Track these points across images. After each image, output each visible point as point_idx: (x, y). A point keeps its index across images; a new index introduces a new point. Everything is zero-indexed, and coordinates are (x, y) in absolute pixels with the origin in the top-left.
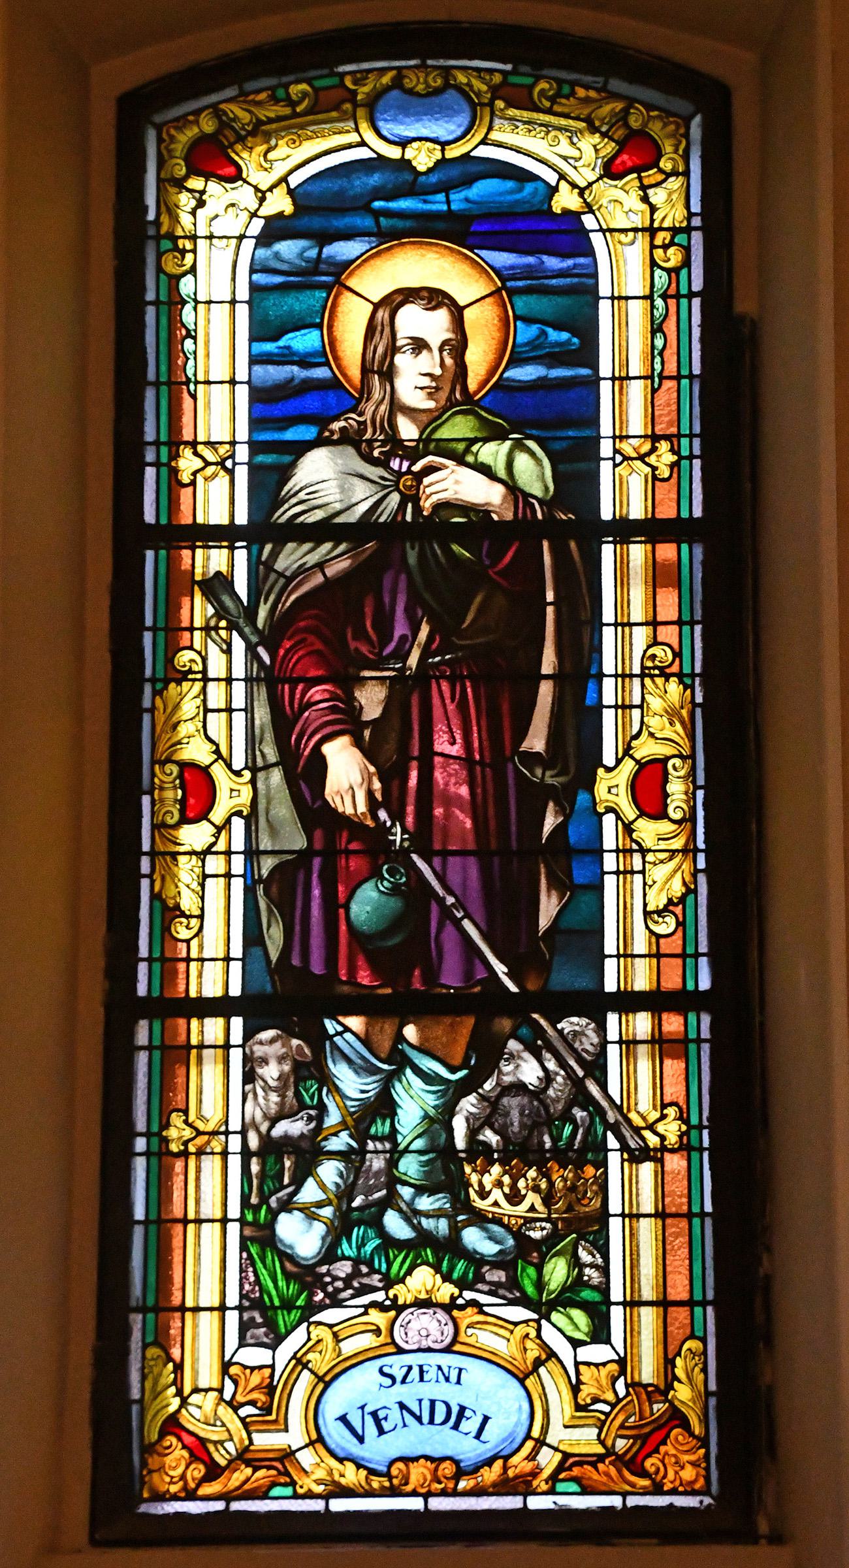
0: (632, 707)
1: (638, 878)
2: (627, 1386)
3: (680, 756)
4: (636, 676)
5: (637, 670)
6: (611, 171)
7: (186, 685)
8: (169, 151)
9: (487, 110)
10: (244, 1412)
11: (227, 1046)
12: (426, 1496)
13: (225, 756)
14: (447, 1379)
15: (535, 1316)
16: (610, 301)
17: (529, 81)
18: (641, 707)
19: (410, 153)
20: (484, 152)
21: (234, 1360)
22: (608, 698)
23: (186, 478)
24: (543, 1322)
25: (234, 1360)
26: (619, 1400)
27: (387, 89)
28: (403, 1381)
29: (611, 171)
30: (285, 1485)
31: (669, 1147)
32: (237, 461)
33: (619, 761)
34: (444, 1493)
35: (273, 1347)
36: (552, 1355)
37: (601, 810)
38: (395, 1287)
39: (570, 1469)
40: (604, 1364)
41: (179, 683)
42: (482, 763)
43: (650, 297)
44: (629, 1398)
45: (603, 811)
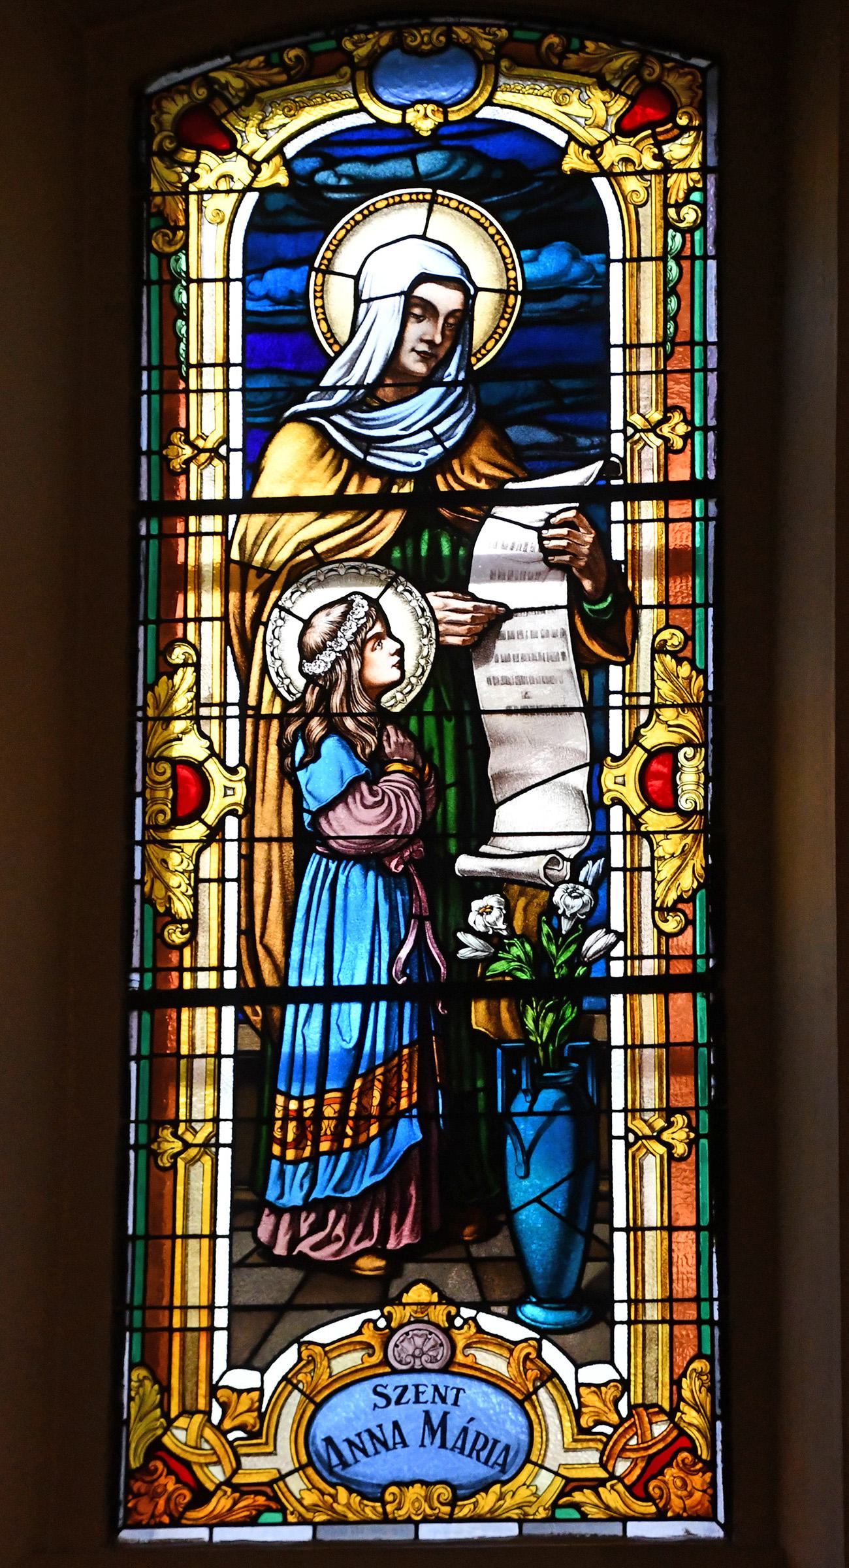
0: (641, 869)
1: (647, 875)
2: (630, 1407)
3: (689, 743)
9: (492, 68)
10: (231, 1436)
11: (226, 390)
13: (217, 751)
17: (534, 36)
18: (651, 869)
19: (411, 117)
20: (488, 113)
21: (221, 1384)
23: (176, 465)
24: (545, 1343)
25: (221, 1384)
28: (398, 1402)
29: (624, 129)
32: (232, 446)
33: (625, 751)
34: (438, 1520)
35: (263, 1371)
39: (569, 1494)
43: (663, 259)
45: (610, 803)
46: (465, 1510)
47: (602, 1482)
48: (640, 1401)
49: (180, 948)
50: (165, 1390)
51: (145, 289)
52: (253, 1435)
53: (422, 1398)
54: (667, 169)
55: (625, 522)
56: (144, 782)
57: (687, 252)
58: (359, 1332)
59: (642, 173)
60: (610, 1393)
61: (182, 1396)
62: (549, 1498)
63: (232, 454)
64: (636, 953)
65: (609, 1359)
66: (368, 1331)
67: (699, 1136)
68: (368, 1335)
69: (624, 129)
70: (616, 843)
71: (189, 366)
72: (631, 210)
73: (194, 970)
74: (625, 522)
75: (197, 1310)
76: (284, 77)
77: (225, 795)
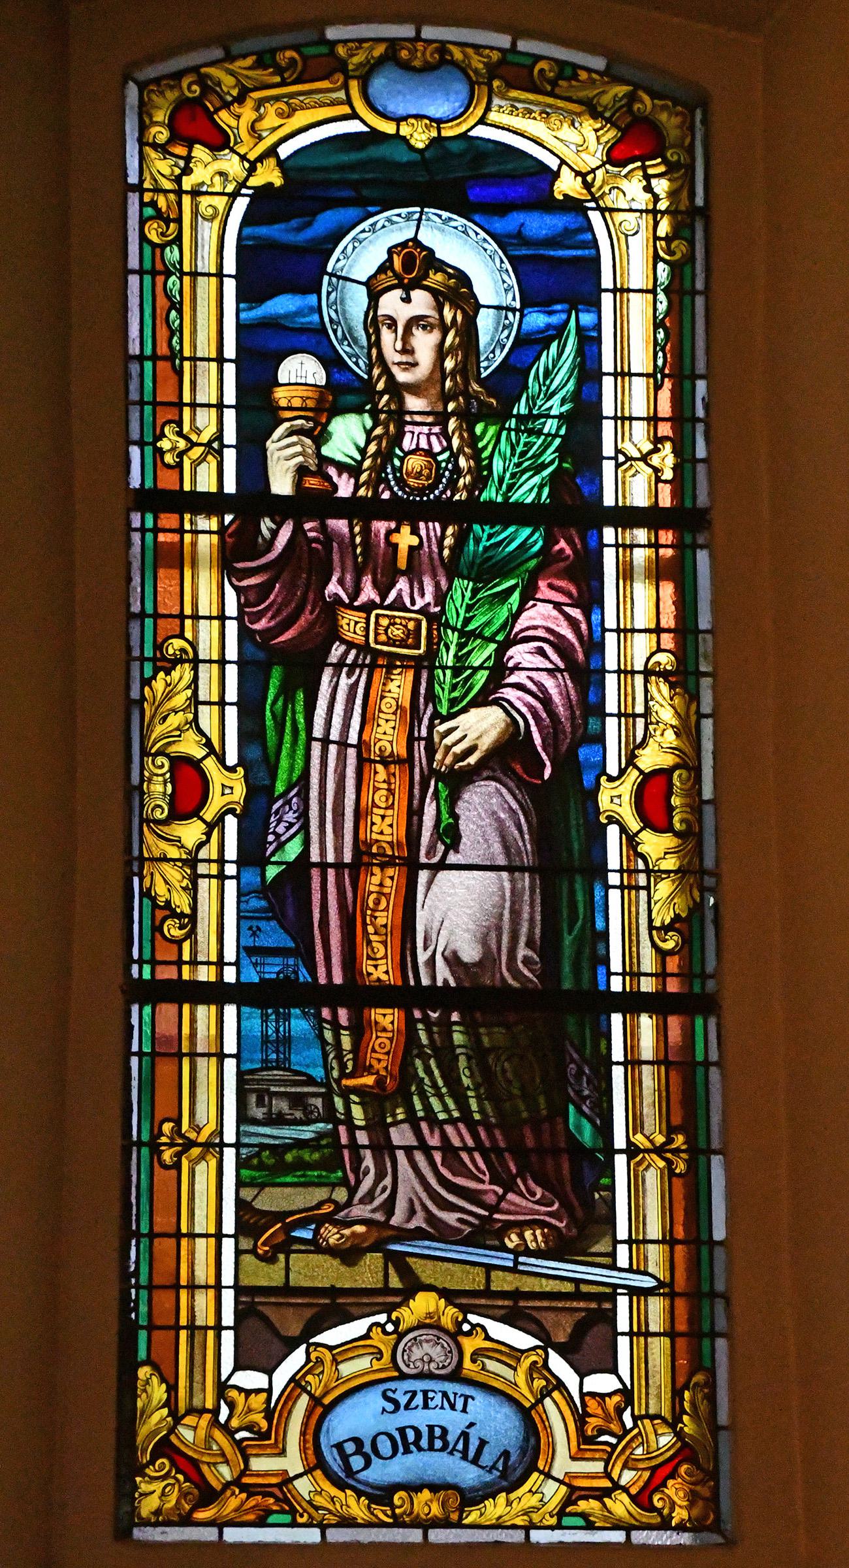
2: (635, 1418)
6: (615, 158)
9: (485, 89)
14: (453, 1407)
16: (613, 421)
19: (405, 130)
20: (481, 132)
21: (231, 1382)
25: (231, 1382)
26: (627, 1432)
28: (407, 1407)
30: (282, 1512)
33: (622, 772)
35: (270, 1372)
36: (560, 1385)
37: (603, 820)
39: (575, 1503)
40: (610, 1395)
42: (485, 1122)
46: (473, 1517)
47: (606, 1493)
48: (643, 1412)
49: (179, 943)
50: (172, 1389)
51: (134, 1242)
53: (431, 1404)
55: (617, 546)
56: (142, 775)
58: (366, 1336)
60: (611, 1403)
62: (553, 1505)
65: (611, 1366)
71: (183, 359)
73: (194, 963)
75: (207, 864)
76: (278, 79)
77: (223, 794)
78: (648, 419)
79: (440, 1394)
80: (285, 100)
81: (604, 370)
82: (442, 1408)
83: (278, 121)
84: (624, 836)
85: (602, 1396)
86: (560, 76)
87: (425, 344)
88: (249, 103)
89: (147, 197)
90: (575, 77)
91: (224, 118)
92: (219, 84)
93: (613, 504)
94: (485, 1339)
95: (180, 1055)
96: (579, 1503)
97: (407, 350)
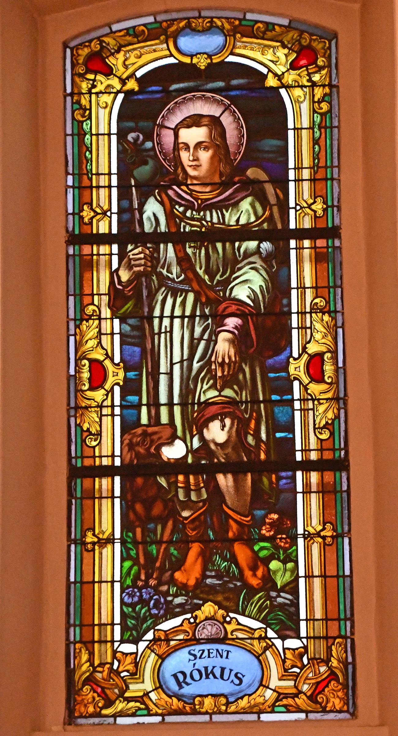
2: (308, 659)
4: (308, 313)
5: (308, 310)
7: (91, 322)
8: (77, 61)
11: (110, 187)
12: (211, 715)
13: (110, 356)
14: (221, 657)
15: (265, 626)
18: (313, 409)
20: (232, 59)
21: (118, 650)
22: (294, 324)
24: (268, 629)
25: (118, 650)
27: (183, 28)
28: (200, 658)
29: (294, 66)
31: (328, 543)
32: (112, 212)
33: (300, 355)
34: (220, 713)
38: (196, 612)
39: (281, 700)
40: (297, 649)
41: (87, 321)
44: (309, 665)
46: (233, 708)
52: (133, 674)
53: (211, 655)
54: (314, 85)
55: (296, 248)
57: (324, 124)
58: (181, 625)
59: (302, 87)
61: (100, 656)
63: (113, 215)
64: (300, 166)
66: (186, 624)
67: (328, 206)
68: (186, 627)
69: (294, 66)
70: (303, 624)
72: (296, 102)
73: (101, 457)
74: (296, 248)
77: (113, 376)
78: (310, 180)
79: (215, 651)
80: (139, 50)
81: (289, 127)
82: (217, 657)
83: (136, 60)
84: (301, 386)
85: (294, 650)
86: (267, 30)
87: (205, 156)
88: (122, 53)
89: (75, 98)
90: (274, 29)
91: (111, 61)
92: (108, 44)
93: (294, 228)
94: (237, 625)
95: (94, 498)
96: (283, 700)
97: (196, 159)
